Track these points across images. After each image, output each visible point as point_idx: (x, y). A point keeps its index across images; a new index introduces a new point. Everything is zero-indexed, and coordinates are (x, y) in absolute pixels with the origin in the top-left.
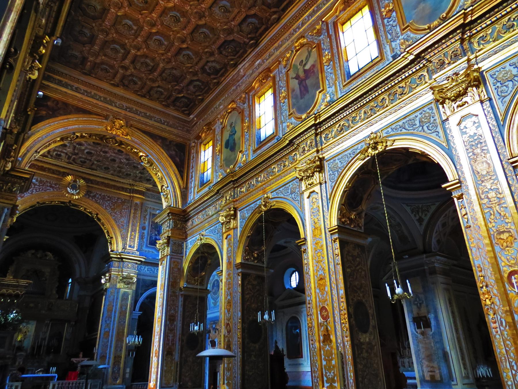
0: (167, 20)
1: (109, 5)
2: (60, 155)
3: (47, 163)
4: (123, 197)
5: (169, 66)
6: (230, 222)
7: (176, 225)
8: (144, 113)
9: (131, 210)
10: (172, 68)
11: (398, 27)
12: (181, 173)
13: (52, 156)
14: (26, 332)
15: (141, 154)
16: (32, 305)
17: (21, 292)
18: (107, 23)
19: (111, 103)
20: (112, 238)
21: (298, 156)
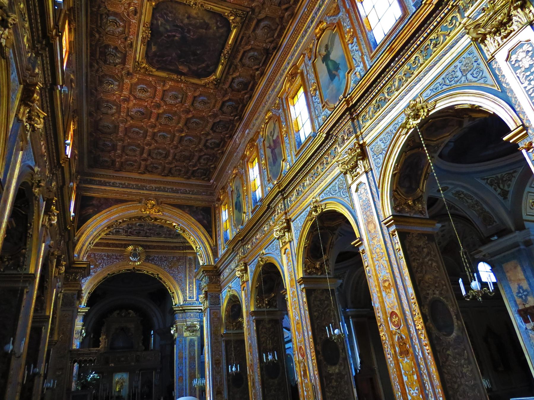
0: (163, 121)
1: (118, 122)
2: (119, 231)
3: (110, 239)
4: (177, 255)
7: (211, 280)
9: (186, 265)
10: (181, 151)
12: (210, 232)
13: (112, 233)
14: (122, 383)
15: (174, 224)
16: (123, 359)
17: (93, 358)
18: (120, 134)
20: (173, 293)
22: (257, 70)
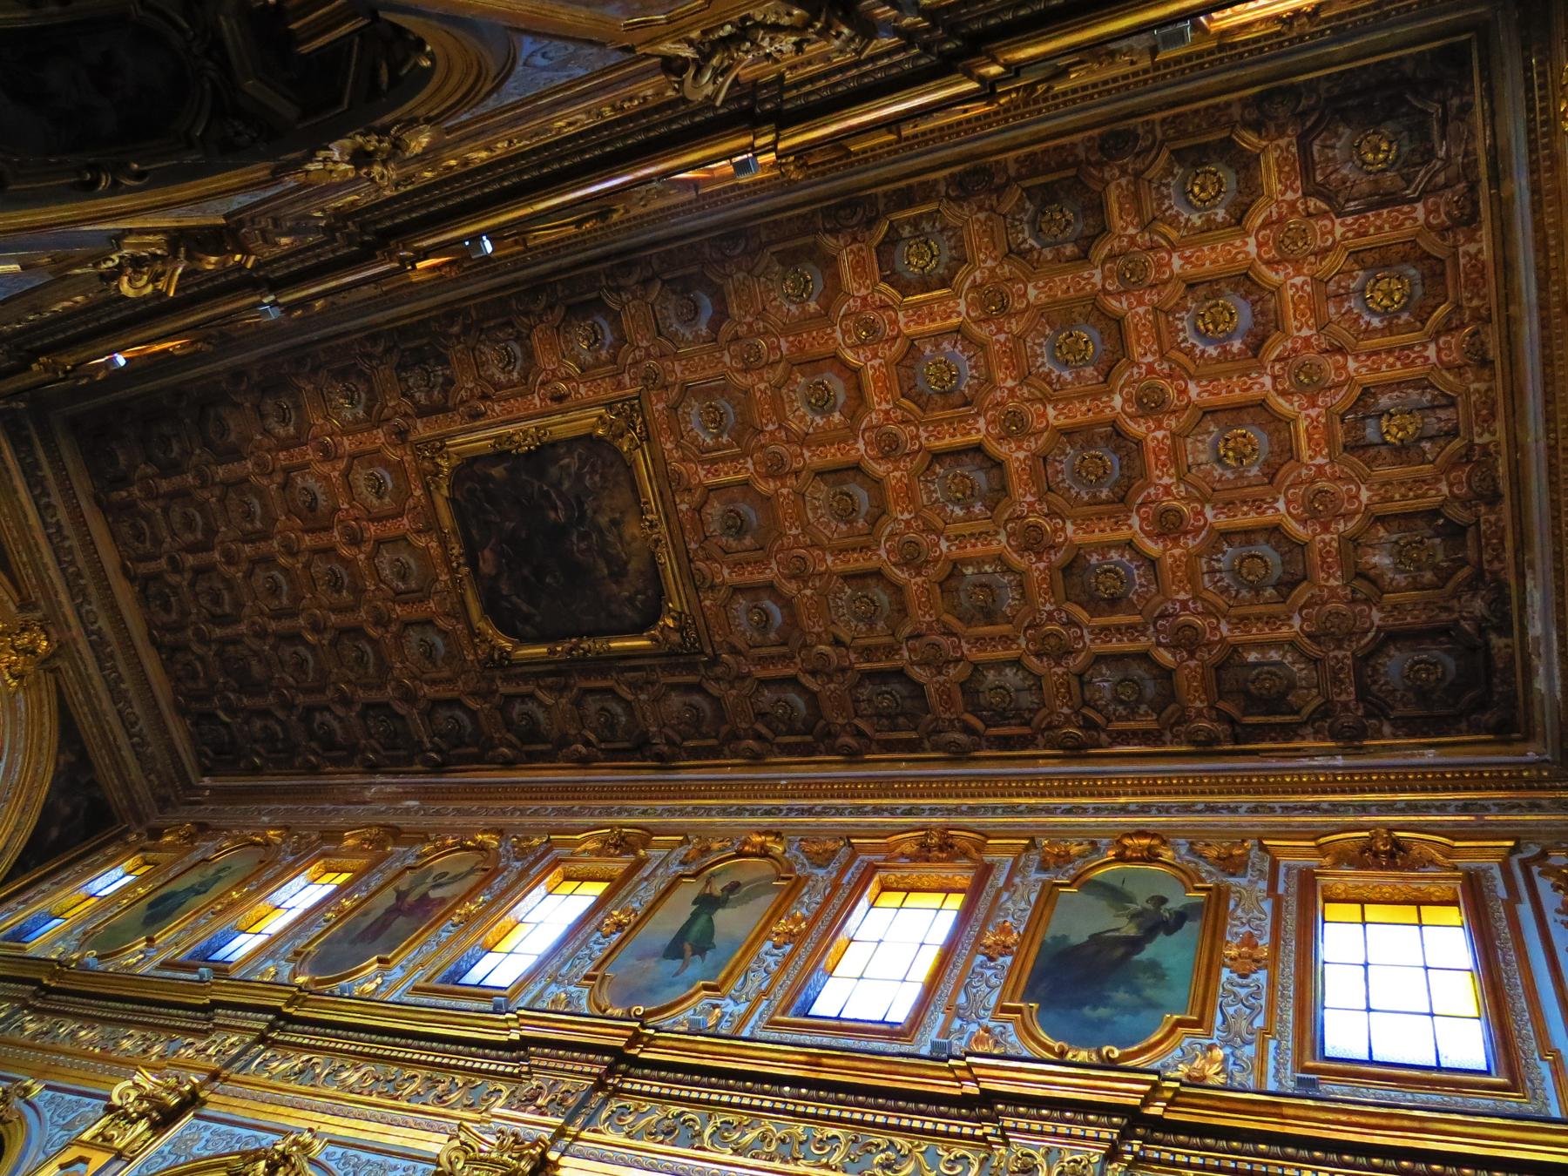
0: (320, 567)
5: (255, 644)
6: (133, 1122)
8: (120, 675)
10: (255, 653)
11: (997, 992)
19: (76, 591)
21: (501, 1102)
22: (587, 743)
